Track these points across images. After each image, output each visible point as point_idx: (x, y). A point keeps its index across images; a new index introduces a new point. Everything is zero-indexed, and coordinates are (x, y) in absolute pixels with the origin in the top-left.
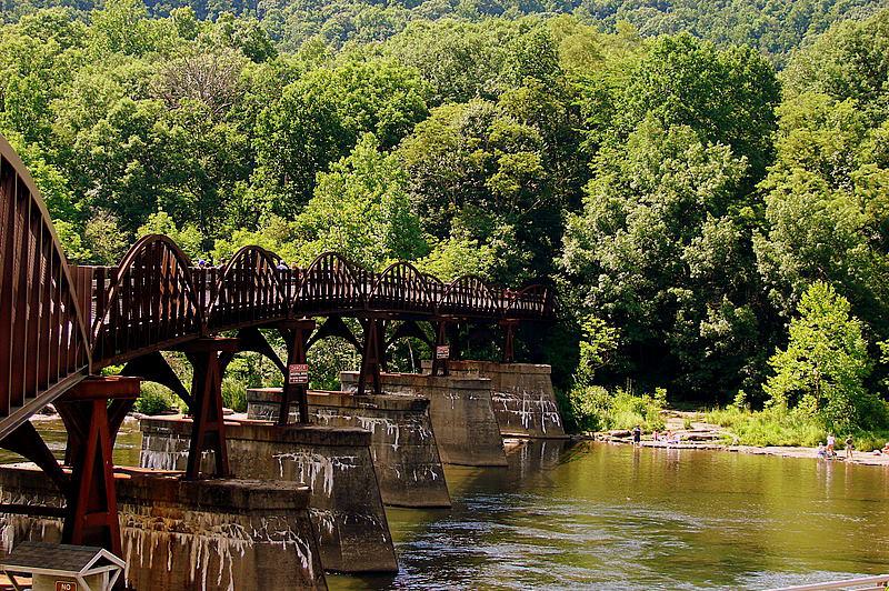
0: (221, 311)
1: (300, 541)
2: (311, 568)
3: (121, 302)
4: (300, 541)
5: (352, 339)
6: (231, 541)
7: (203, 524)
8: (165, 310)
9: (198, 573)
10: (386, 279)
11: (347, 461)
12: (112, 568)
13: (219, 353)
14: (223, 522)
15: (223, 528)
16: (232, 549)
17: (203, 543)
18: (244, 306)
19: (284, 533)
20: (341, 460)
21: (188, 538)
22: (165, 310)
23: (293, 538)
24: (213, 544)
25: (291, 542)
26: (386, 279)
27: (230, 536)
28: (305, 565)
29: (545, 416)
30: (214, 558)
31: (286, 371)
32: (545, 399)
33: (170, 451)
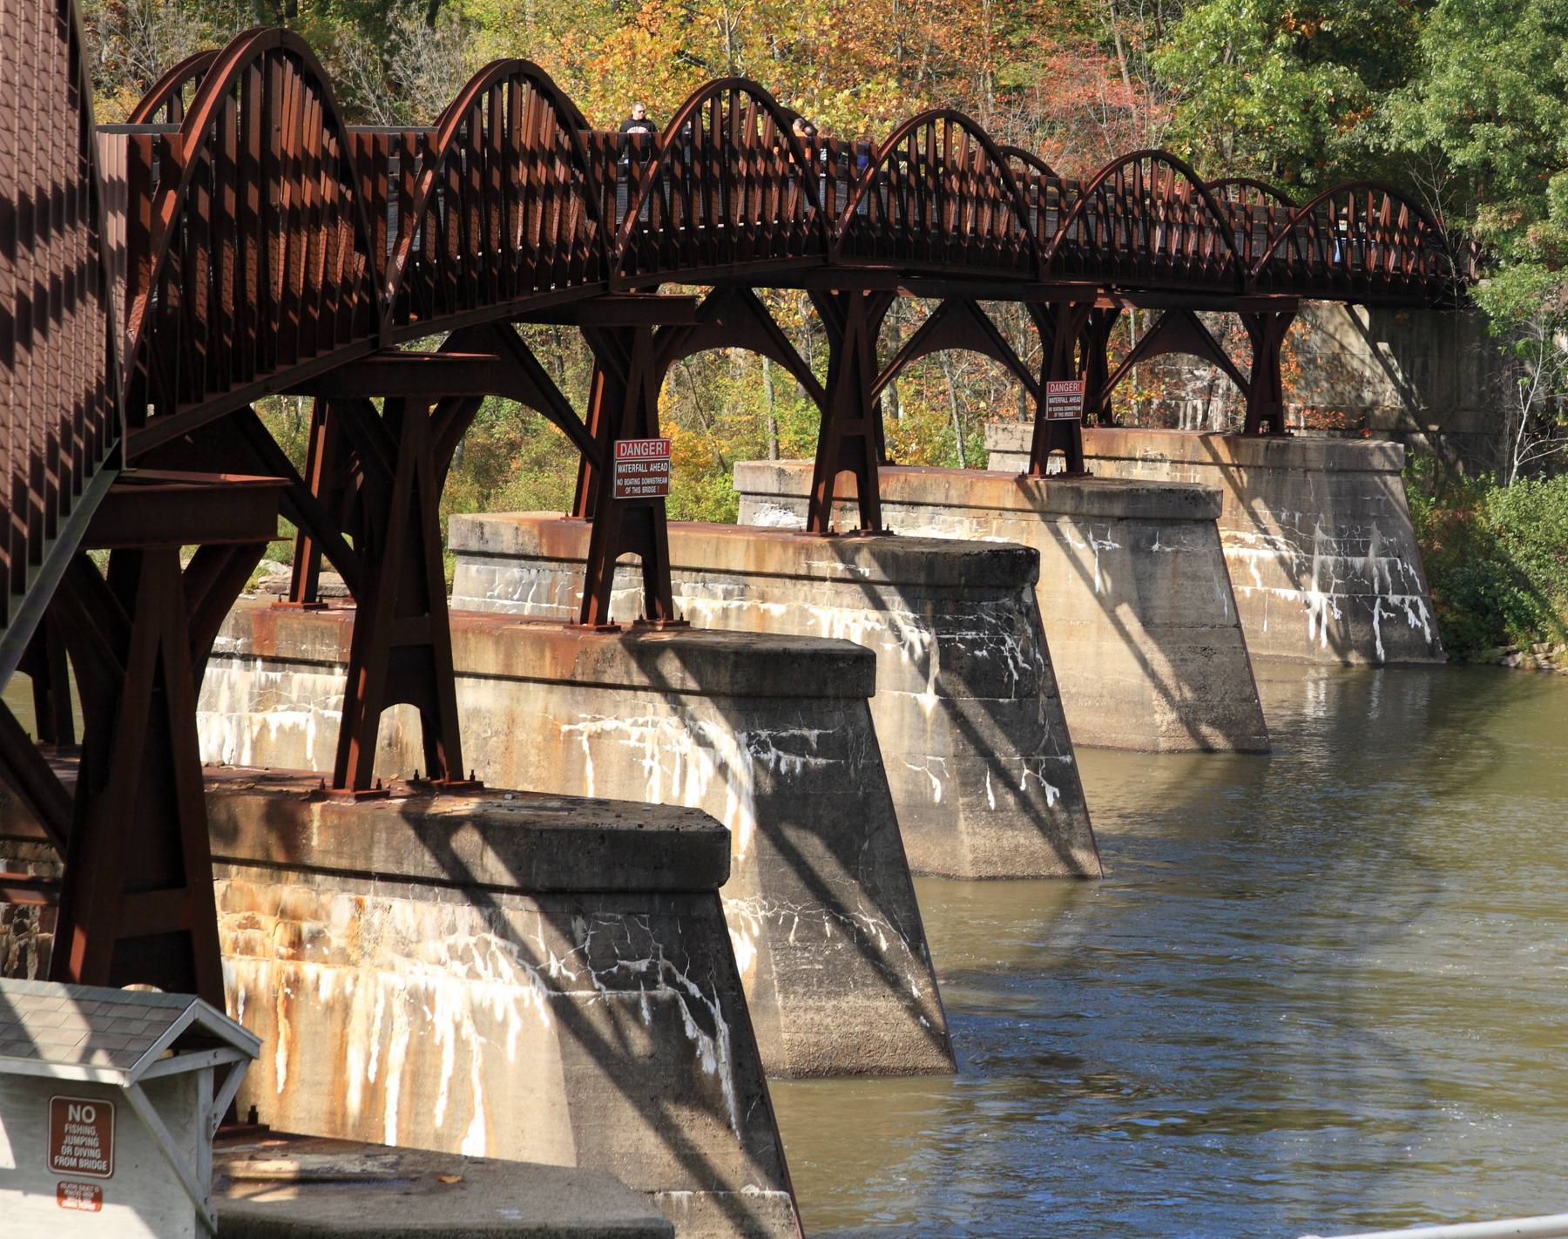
0: (653, 232)
1: (694, 989)
2: (725, 1072)
3: (186, 231)
4: (694, 989)
5: (558, 409)
6: (475, 984)
7: (389, 935)
8: (486, 232)
9: (373, 1092)
10: (894, 166)
11: (798, 746)
12: (223, 1057)
13: (433, 407)
14: (453, 929)
15: (451, 949)
16: (481, 1016)
17: (390, 993)
18: (711, 227)
19: (643, 965)
20: (780, 744)
21: (339, 981)
22: (486, 232)
23: (670, 980)
24: (420, 1001)
25: (664, 992)
26: (894, 166)
27: (473, 974)
28: (708, 1066)
29: (1386, 606)
30: (420, 1054)
31: (1039, 394)
32: (1384, 551)
33: (232, 708)
